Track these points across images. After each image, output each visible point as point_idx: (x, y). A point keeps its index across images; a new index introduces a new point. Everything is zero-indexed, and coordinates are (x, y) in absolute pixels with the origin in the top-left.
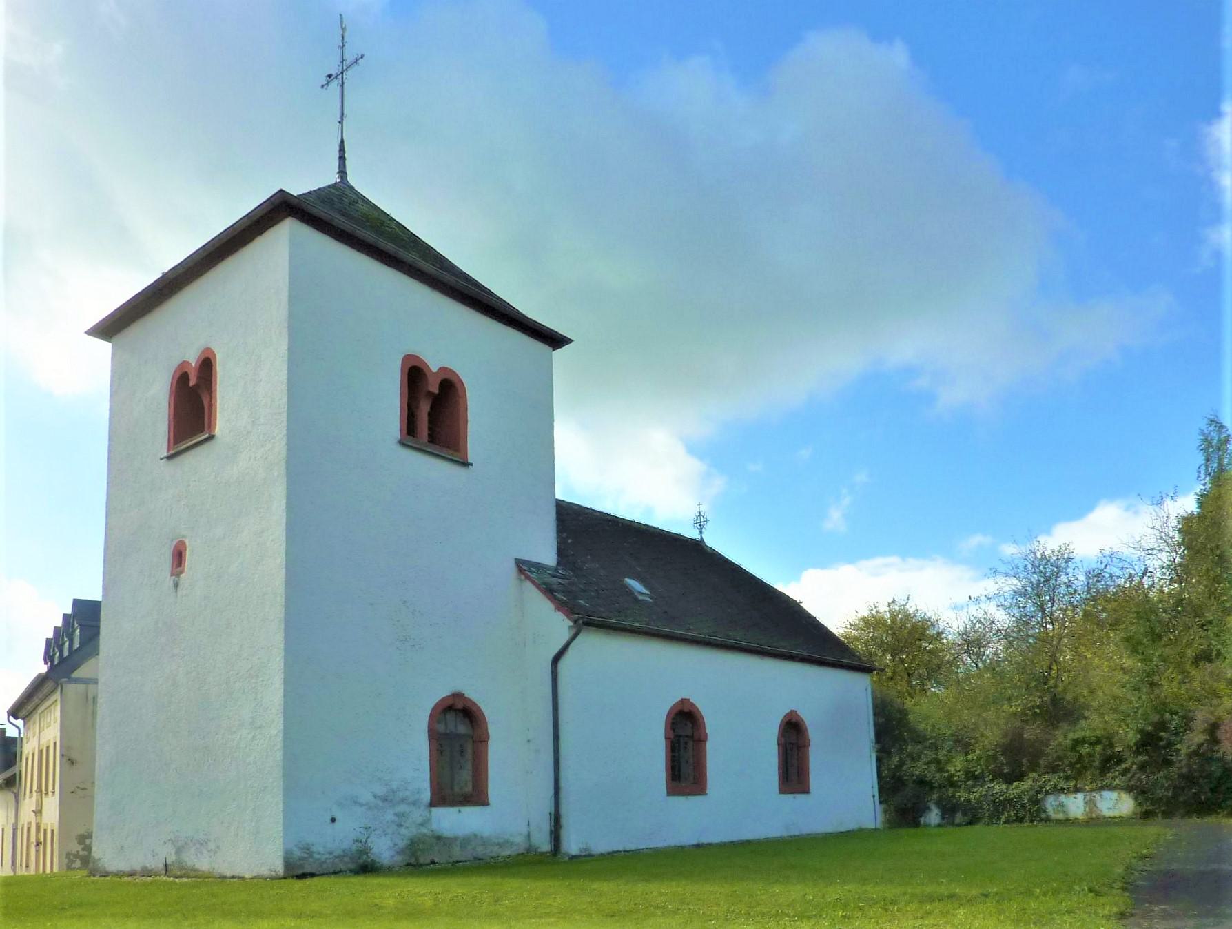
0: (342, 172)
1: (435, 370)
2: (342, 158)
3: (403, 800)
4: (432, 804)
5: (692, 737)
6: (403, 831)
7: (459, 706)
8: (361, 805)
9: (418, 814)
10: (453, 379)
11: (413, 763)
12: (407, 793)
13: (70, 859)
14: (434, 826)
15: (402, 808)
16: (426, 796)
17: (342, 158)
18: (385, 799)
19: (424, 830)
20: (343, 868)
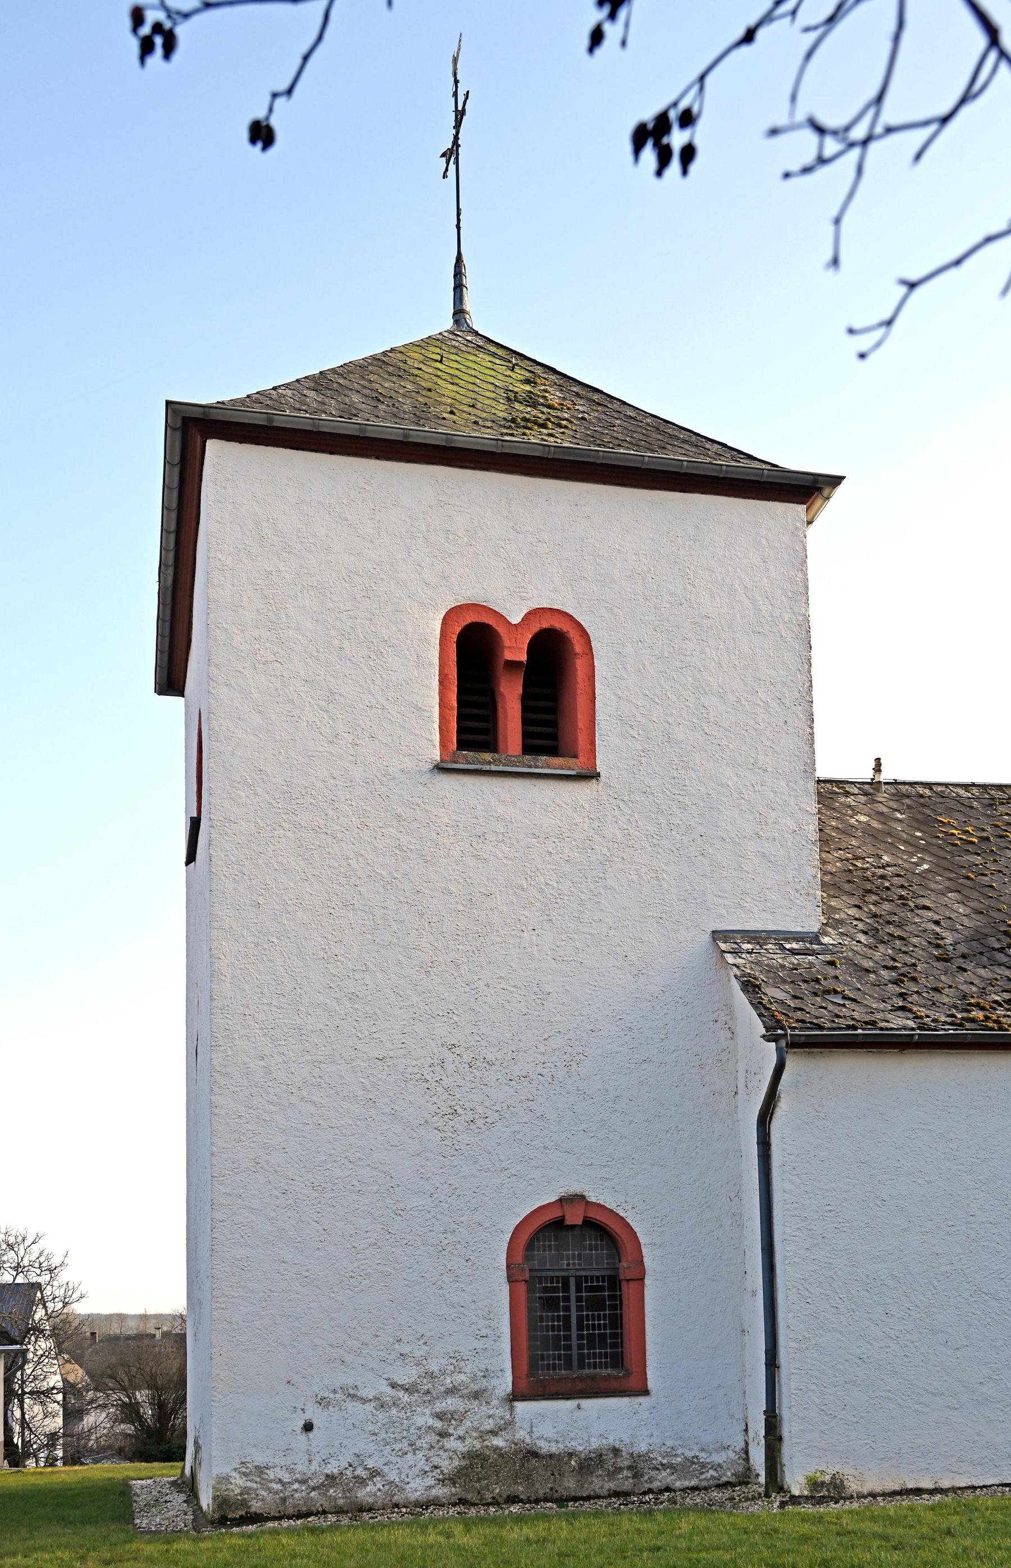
0: (459, 313)
1: (516, 619)
2: (459, 287)
3: (452, 1391)
4: (516, 1396)
6: (451, 1443)
8: (364, 1401)
9: (484, 1415)
10: (558, 624)
11: (482, 1325)
12: (463, 1377)
14: (521, 1434)
15: (451, 1403)
16: (505, 1383)
17: (459, 287)
18: (410, 1389)
19: (499, 1442)
20: (327, 1506)
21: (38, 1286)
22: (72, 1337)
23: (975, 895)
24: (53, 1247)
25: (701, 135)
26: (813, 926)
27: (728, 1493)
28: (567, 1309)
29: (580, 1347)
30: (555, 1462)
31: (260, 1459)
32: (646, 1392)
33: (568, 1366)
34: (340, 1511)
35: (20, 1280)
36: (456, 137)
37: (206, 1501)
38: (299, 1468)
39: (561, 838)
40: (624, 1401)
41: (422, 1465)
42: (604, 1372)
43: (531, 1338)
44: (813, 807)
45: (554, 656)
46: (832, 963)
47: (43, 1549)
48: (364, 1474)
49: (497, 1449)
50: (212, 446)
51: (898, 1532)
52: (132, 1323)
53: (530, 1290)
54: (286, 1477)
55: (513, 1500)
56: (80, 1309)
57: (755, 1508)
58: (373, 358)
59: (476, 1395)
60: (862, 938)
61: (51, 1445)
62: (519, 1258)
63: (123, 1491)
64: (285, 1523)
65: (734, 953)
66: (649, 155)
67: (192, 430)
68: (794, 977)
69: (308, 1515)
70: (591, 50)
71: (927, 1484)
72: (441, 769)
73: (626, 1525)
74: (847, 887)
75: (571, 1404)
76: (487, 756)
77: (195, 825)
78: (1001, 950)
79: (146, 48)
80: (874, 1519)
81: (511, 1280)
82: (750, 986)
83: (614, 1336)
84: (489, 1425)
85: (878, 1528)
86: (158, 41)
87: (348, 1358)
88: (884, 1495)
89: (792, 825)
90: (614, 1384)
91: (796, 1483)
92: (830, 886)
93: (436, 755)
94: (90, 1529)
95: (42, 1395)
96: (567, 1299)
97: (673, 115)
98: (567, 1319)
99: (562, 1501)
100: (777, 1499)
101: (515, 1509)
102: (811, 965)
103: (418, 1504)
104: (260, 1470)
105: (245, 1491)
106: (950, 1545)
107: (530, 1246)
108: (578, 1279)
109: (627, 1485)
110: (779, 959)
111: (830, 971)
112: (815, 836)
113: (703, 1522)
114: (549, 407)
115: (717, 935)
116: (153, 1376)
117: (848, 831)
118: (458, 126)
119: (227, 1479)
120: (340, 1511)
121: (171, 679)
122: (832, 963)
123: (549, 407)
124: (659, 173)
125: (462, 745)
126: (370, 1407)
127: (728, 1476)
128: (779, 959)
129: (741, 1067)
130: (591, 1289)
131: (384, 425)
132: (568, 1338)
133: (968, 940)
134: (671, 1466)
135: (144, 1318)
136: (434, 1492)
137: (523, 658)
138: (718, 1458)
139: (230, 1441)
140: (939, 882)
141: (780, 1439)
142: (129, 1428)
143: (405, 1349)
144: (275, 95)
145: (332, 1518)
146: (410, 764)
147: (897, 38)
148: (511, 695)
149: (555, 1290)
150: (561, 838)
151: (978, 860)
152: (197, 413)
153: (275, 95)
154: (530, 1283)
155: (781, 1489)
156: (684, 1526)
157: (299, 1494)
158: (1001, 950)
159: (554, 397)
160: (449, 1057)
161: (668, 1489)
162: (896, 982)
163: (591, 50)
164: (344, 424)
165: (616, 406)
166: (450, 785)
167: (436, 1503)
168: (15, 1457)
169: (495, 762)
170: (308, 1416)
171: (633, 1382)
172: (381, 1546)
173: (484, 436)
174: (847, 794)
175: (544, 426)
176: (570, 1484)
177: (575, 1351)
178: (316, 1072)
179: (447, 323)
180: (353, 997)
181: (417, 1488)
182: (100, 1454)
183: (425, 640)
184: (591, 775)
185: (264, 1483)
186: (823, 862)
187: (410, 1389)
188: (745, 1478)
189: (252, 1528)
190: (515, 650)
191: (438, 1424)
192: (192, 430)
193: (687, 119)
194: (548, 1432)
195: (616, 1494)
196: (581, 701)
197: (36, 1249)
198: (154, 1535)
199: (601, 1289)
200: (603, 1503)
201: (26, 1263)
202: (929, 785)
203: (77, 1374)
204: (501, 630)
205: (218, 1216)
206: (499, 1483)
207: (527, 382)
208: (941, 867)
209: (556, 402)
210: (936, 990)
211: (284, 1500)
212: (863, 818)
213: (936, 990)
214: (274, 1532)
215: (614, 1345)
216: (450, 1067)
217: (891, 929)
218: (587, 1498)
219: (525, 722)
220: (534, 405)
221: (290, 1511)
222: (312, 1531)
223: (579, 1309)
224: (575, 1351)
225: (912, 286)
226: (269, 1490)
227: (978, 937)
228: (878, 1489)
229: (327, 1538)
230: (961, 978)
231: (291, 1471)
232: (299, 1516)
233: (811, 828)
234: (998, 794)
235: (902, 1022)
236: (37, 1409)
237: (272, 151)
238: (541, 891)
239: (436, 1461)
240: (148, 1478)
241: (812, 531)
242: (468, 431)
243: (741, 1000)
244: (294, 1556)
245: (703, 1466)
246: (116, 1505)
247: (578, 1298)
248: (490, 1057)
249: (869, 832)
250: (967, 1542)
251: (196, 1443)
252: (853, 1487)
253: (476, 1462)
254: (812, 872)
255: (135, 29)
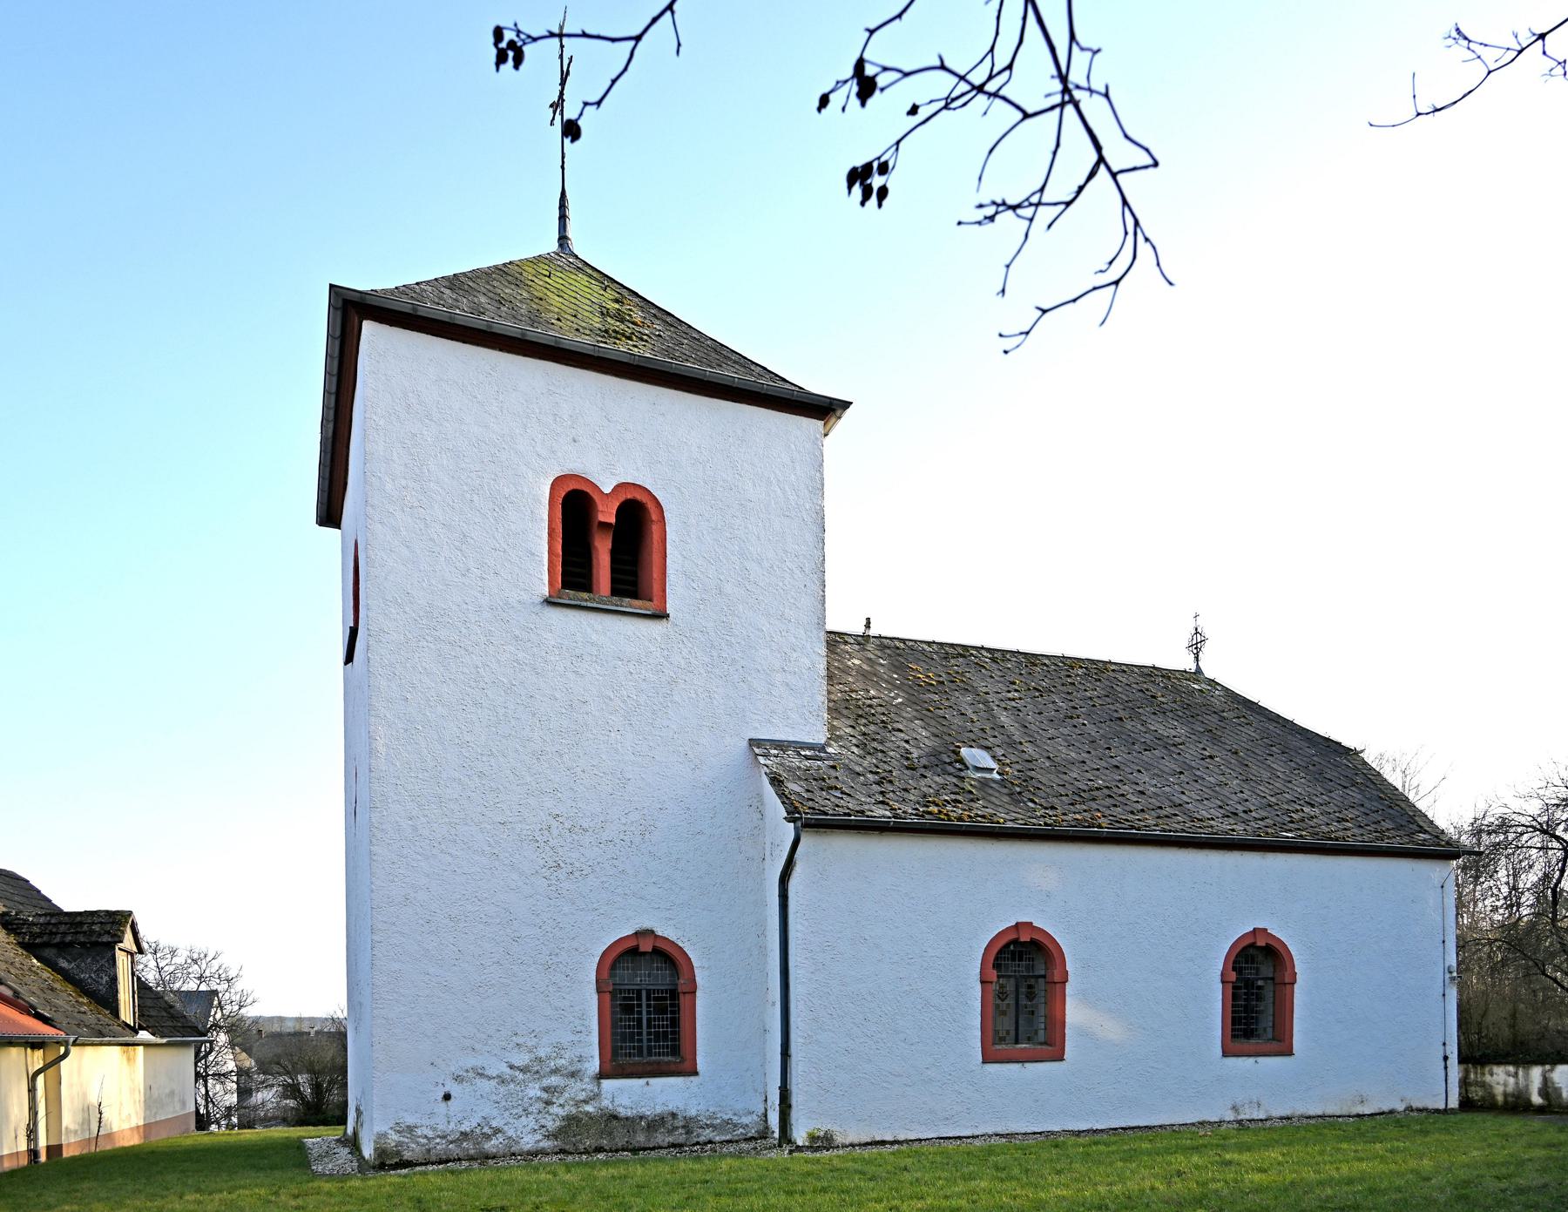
0: (563, 239)
1: (607, 490)
2: (563, 218)
3: (555, 1071)
4: (602, 1075)
5: (1044, 977)
6: (555, 1109)
7: (646, 946)
8: (490, 1078)
9: (579, 1089)
10: (639, 497)
13: (30, 1161)
14: (606, 1103)
15: (554, 1080)
16: (594, 1066)
17: (563, 218)
18: (523, 1070)
19: (589, 1108)
21: (215, 993)
22: (243, 1033)
23: (933, 723)
24: (230, 962)
25: (893, 181)
26: (820, 737)
27: (752, 1145)
28: (640, 1013)
29: (649, 1040)
30: (630, 1123)
31: (410, 1120)
32: (695, 1073)
33: (640, 1054)
34: (471, 1159)
35: (203, 987)
36: (562, 93)
37: (368, 1151)
38: (440, 1127)
39: (639, 661)
40: (680, 1079)
41: (533, 1125)
42: (666, 1059)
43: (614, 1034)
44: (823, 650)
45: (636, 519)
46: (834, 767)
47: (244, 1187)
48: (490, 1132)
49: (587, 1113)
50: (368, 327)
51: (871, 1169)
52: (290, 1024)
53: (613, 998)
54: (430, 1134)
55: (599, 1150)
56: (250, 1012)
57: (773, 1154)
58: (496, 267)
59: (573, 1075)
60: (855, 750)
61: (228, 1116)
62: (605, 974)
63: (299, 1146)
64: (430, 1168)
65: (765, 756)
66: (857, 190)
67: (351, 311)
68: (807, 776)
69: (447, 1161)
70: (819, 110)
71: (889, 1138)
72: (549, 602)
73: (682, 1166)
74: (845, 712)
75: (642, 1081)
76: (585, 595)
77: (354, 632)
78: (950, 764)
79: (501, 59)
80: (854, 1160)
81: (599, 991)
82: (776, 781)
83: (673, 1033)
84: (582, 1096)
85: (858, 1166)
86: (511, 54)
87: (477, 1046)
88: (860, 1145)
89: (807, 662)
90: (673, 1067)
91: (800, 1136)
92: (834, 710)
93: (546, 591)
94: (277, 1174)
95: (219, 1076)
96: (640, 1006)
97: (875, 165)
98: (640, 1021)
99: (635, 1151)
100: (786, 1148)
101: (601, 1156)
102: (819, 768)
103: (529, 1153)
104: (410, 1129)
105: (399, 1144)
106: (907, 1176)
107: (613, 967)
108: (648, 992)
109: (681, 1139)
110: (796, 762)
111: (833, 773)
112: (824, 673)
113: (736, 1163)
114: (634, 323)
115: (754, 743)
116: (311, 1063)
117: (846, 670)
118: (563, 83)
119: (385, 1135)
120: (471, 1159)
121: (330, 514)
122: (834, 767)
123: (634, 323)
124: (863, 204)
125: (565, 585)
126: (493, 1083)
127: (753, 1133)
128: (796, 762)
129: (768, 841)
130: (656, 999)
131: (506, 324)
132: (640, 1034)
133: (929, 755)
134: (712, 1126)
135: (300, 1020)
136: (541, 1144)
137: (613, 520)
138: (745, 1120)
139: (384, 1106)
140: (909, 712)
141: (790, 1106)
142: (291, 1103)
143: (520, 1040)
144: (586, 104)
145: (465, 1164)
146: (525, 597)
147: (1055, 153)
148: (603, 549)
149: (631, 999)
150: (639, 661)
151: (936, 697)
152: (356, 297)
153: (586, 104)
154: (613, 994)
155: (790, 1142)
156: (724, 1165)
157: (440, 1147)
158: (950, 764)
159: (638, 316)
160: (554, 824)
161: (710, 1142)
162: (878, 783)
163: (819, 110)
164: (469, 316)
165: (684, 328)
166: (556, 616)
167: (544, 1152)
168: (202, 1122)
169: (590, 600)
170: (447, 1089)
171: (687, 1065)
172: (505, 1182)
173: (585, 341)
174: (846, 643)
175: (630, 338)
176: (641, 1138)
177: (645, 1043)
178: (453, 831)
179: (552, 246)
180: (481, 774)
181: (529, 1142)
182: (267, 1121)
183: (538, 501)
184: (661, 615)
185: (414, 1138)
186: (829, 692)
187: (523, 1070)
188: (764, 1134)
189: (404, 1171)
190: (607, 514)
191: (545, 1096)
192: (351, 311)
193: (884, 169)
194: (626, 1102)
195: (674, 1145)
196: (656, 557)
197: (215, 964)
198: (331, 1177)
199: (665, 999)
200: (664, 1152)
201: (207, 973)
202: (903, 641)
203: (249, 1063)
204: (596, 497)
205: (376, 938)
206: (589, 1137)
207: (617, 301)
208: (912, 701)
209: (638, 320)
210: (905, 790)
211: (429, 1151)
212: (857, 662)
213: (905, 790)
214: (425, 1173)
215: (673, 1040)
216: (555, 832)
217: (875, 744)
218: (653, 1149)
219: (613, 571)
220: (622, 321)
221: (434, 1158)
222: (452, 1172)
223: (649, 1013)
224: (645, 1043)
225: (1044, 311)
226: (418, 1143)
227: (935, 754)
228: (856, 1141)
229: (465, 1178)
230: (923, 782)
231: (434, 1129)
232: (440, 1163)
233: (821, 666)
234: (951, 650)
235: (882, 812)
236: (218, 1087)
237: (577, 143)
238: (624, 702)
239: (543, 1122)
240: (316, 1138)
241: (827, 441)
242: (571, 336)
243: (769, 791)
244: (442, 1190)
245: (735, 1125)
246: (297, 1156)
247: (647, 1004)
248: (585, 825)
249: (862, 674)
250: (919, 1175)
251: (358, 1110)
252: (839, 1139)
253: (572, 1123)
254: (821, 699)
255: (496, 44)
